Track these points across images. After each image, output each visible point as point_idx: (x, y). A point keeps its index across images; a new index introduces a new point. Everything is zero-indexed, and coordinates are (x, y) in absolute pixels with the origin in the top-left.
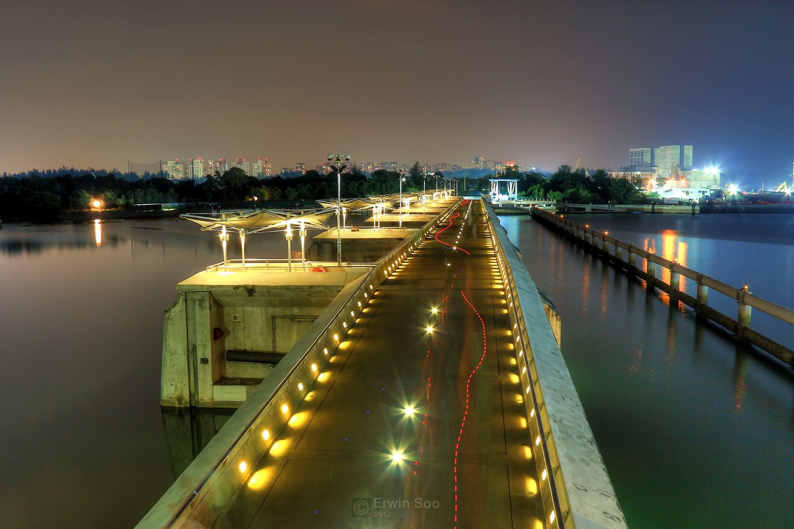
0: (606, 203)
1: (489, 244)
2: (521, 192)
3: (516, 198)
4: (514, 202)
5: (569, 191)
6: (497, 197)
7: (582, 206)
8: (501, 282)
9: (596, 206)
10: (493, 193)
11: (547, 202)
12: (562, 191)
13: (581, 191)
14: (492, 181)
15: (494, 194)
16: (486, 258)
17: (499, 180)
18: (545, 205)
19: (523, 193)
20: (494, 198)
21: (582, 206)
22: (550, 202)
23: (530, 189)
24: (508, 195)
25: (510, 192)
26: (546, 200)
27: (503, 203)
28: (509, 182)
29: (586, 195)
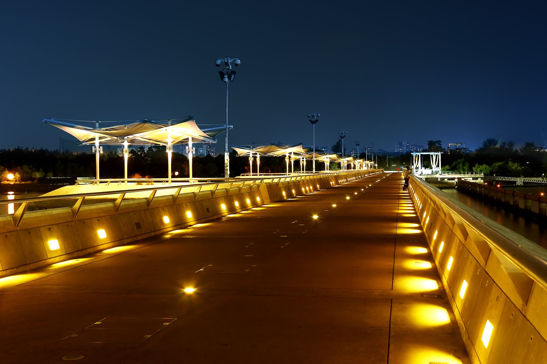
0: (539, 175)
1: (405, 209)
2: (445, 166)
3: (440, 172)
4: (437, 176)
5: (497, 165)
6: (420, 170)
7: (512, 179)
8: (426, 265)
9: (528, 179)
10: (415, 166)
11: (473, 176)
12: (489, 164)
13: (510, 164)
14: (414, 154)
15: (417, 168)
16: (390, 249)
17: (422, 153)
18: (471, 179)
19: (447, 167)
20: (417, 171)
21: (512, 179)
22: (477, 176)
23: (454, 164)
24: (431, 168)
25: (434, 166)
26: (472, 173)
27: (426, 177)
28: (432, 156)
29: (516, 168)
